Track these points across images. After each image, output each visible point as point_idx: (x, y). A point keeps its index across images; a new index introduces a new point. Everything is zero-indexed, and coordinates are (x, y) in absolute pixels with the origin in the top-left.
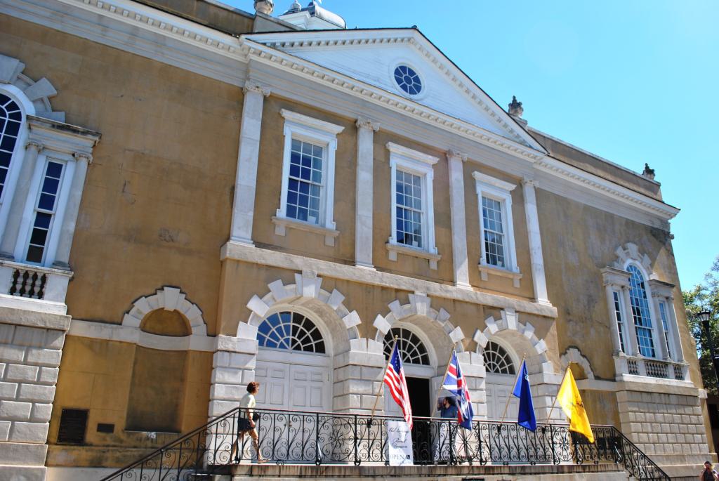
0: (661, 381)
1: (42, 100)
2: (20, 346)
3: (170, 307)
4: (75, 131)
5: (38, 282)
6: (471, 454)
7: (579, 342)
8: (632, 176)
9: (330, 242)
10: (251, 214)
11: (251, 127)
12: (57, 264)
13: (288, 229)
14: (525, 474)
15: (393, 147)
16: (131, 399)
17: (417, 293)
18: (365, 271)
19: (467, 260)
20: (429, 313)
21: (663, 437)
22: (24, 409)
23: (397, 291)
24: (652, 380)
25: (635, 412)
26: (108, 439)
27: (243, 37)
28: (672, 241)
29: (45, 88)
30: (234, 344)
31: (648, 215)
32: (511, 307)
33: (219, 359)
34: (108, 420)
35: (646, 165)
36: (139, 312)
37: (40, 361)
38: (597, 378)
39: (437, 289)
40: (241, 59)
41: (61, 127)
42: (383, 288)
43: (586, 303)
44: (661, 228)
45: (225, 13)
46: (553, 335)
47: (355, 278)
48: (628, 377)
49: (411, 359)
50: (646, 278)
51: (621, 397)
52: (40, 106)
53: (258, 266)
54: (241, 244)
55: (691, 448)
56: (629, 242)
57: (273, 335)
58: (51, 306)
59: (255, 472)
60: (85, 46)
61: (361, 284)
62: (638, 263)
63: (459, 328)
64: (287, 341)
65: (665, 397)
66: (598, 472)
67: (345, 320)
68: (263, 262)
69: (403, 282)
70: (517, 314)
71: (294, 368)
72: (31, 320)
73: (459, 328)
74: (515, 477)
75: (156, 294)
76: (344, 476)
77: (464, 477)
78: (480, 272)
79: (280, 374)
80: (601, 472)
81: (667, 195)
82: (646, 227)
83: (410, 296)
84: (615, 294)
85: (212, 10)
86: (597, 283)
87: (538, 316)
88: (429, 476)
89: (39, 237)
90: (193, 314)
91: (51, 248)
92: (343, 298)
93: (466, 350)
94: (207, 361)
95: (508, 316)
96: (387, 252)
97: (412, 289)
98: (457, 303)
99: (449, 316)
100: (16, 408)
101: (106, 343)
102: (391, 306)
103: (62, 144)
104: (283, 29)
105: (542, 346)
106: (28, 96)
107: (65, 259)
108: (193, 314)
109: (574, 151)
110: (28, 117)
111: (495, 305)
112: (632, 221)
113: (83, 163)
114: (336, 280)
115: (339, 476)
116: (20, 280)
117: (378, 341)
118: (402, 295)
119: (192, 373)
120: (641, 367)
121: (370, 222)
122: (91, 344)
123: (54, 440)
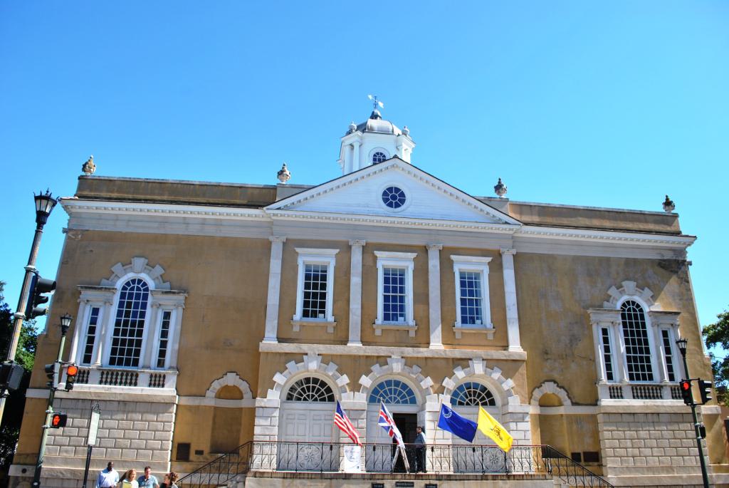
0: (658, 402)
1: (157, 278)
2: (154, 413)
3: (231, 384)
4: (174, 293)
5: (162, 379)
6: (565, 468)
7: (556, 376)
8: (640, 216)
9: (331, 330)
10: (276, 321)
11: (275, 266)
12: (170, 368)
13: (302, 326)
14: (450, 480)
15: (377, 253)
16: (213, 436)
17: (393, 356)
18: (355, 347)
19: (440, 326)
20: (403, 369)
21: (648, 451)
22: (157, 444)
23: (378, 357)
24: (638, 403)
25: (611, 431)
26: (201, 458)
27: (265, 208)
28: (66, 227)
29: (159, 270)
30: (265, 403)
31: (653, 249)
32: (478, 357)
33: (258, 412)
34: (200, 449)
35: (667, 196)
36: (214, 389)
37: (164, 420)
38: (574, 404)
39: (409, 352)
40: (269, 220)
41: (166, 293)
42: (367, 357)
43: (568, 342)
44: (674, 258)
45: (258, 190)
46: (522, 375)
47: (345, 353)
48: (606, 402)
49: (401, 401)
50: (646, 309)
51: (600, 418)
52: (157, 281)
53: (280, 354)
54: (270, 343)
55: (683, 460)
56: (627, 279)
57: (319, 390)
58: (168, 391)
59: (257, 475)
60: (178, 239)
61: (350, 356)
62: (637, 299)
63: (429, 378)
64: (308, 396)
65: (655, 417)
66: (523, 480)
67: (338, 381)
68: (283, 351)
69: (382, 351)
70: (485, 362)
71: (313, 413)
72: (158, 400)
73: (429, 378)
74: (441, 482)
75: (223, 377)
76: (311, 478)
77: (427, 482)
78: (454, 333)
79: (304, 417)
80: (527, 480)
81: (685, 226)
82: (652, 261)
83: (388, 359)
84: (605, 331)
85: (250, 191)
86: (584, 323)
87: (506, 360)
88: (370, 479)
89: (162, 354)
90: (244, 386)
91: (168, 359)
92: (336, 367)
93: (435, 393)
94: (252, 412)
95: (475, 365)
96: (374, 330)
97: (390, 354)
98: (429, 361)
99: (420, 370)
100: (154, 444)
101: (198, 407)
102: (372, 368)
103: (170, 302)
104: (297, 191)
105: (509, 384)
106: (150, 277)
107: (174, 365)
108: (244, 386)
109: (564, 210)
110: (151, 291)
111: (463, 357)
112: (634, 259)
113: (180, 310)
114: (332, 356)
115: (308, 478)
116: (153, 379)
117: (362, 393)
118: (382, 360)
119: (244, 420)
120: (627, 392)
121: (359, 312)
122: (190, 408)
123: (174, 459)
